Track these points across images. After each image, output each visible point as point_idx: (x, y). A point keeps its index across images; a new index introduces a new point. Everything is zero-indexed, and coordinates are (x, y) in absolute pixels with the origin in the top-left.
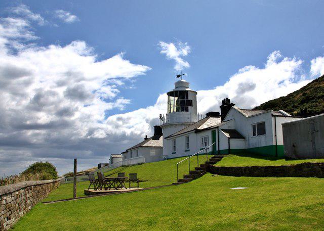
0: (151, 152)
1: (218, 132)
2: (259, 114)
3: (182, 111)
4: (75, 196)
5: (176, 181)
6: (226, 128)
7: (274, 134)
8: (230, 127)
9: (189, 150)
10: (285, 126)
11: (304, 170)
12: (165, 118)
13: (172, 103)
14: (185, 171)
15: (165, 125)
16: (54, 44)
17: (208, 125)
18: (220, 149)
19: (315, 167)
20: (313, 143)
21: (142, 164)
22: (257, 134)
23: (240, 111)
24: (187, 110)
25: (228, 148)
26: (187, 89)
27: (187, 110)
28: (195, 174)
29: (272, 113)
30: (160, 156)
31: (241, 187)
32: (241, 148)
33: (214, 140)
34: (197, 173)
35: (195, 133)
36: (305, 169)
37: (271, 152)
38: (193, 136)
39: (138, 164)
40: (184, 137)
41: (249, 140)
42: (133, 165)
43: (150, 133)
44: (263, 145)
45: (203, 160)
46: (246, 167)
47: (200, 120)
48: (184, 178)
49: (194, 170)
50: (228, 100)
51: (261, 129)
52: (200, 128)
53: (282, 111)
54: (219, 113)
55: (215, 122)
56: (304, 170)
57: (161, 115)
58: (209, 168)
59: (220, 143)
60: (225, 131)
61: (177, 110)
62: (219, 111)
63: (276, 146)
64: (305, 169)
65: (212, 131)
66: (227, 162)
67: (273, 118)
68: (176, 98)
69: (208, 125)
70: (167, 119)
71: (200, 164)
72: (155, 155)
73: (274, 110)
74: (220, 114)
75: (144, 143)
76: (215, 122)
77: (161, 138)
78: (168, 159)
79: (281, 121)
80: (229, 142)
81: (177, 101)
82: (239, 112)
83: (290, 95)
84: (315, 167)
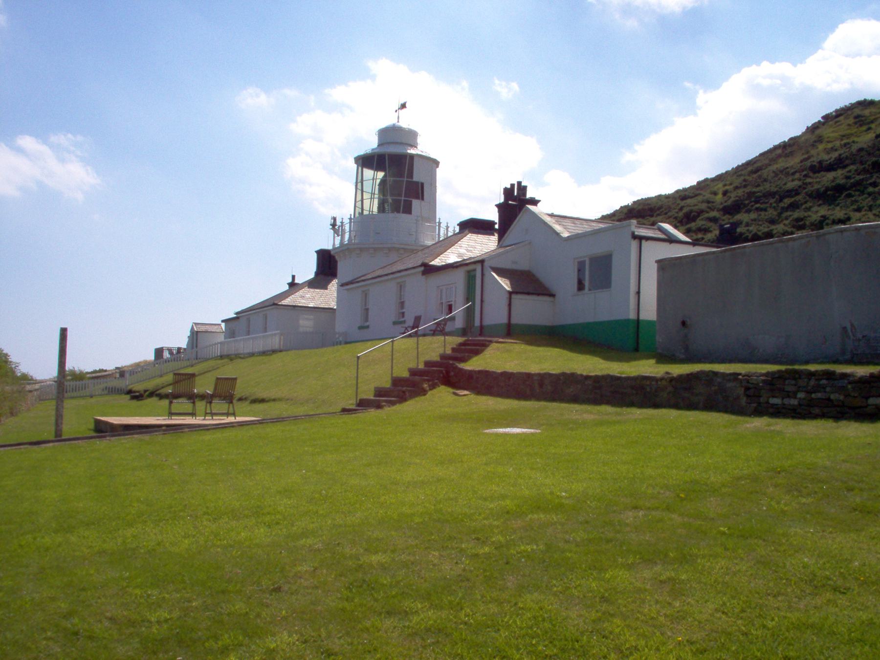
0: (301, 322)
1: (483, 275)
4: (58, 433)
5: (351, 404)
6: (508, 265)
7: (633, 288)
9: (368, 327)
10: (663, 265)
12: (347, 228)
13: (368, 187)
14: (379, 376)
15: (345, 249)
16: (768, 60)
17: (460, 255)
19: (730, 385)
21: (274, 351)
22: (587, 284)
23: (548, 220)
24: (408, 210)
26: (411, 151)
28: (404, 388)
29: (633, 228)
30: (324, 332)
31: (516, 426)
33: (469, 296)
34: (414, 384)
35: (424, 273)
37: (626, 339)
38: (417, 284)
39: (264, 353)
42: (252, 355)
43: (308, 270)
45: (435, 348)
46: (545, 374)
47: (450, 234)
48: (375, 396)
49: (406, 374)
50: (522, 189)
52: (437, 262)
53: (667, 226)
54: (493, 223)
55: (481, 246)
57: (335, 219)
58: (446, 374)
59: (485, 305)
60: (502, 272)
61: (382, 208)
62: (493, 215)
63: (638, 321)
65: (469, 272)
66: (502, 358)
67: (634, 244)
68: (381, 175)
69: (460, 255)
70: (350, 231)
71: (422, 359)
72: (311, 330)
73: (639, 223)
74: (497, 227)
75: (284, 295)
76: (481, 246)
77: (334, 285)
78: (346, 343)
79: (655, 253)
80: (510, 305)
81: (383, 182)
84: (730, 385)
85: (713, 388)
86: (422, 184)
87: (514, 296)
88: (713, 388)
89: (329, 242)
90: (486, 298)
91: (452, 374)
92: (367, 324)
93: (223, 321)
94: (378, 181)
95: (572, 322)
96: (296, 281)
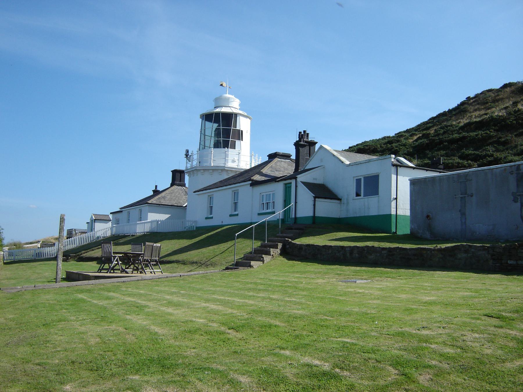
1: (296, 186)
2: (369, 161)
3: (224, 147)
8: (316, 179)
9: (237, 215)
11: (459, 256)
15: (193, 171)
18: (298, 215)
20: (463, 214)
23: (335, 153)
25: (311, 214)
27: (233, 147)
32: (176, 231)
35: (251, 185)
36: (461, 255)
40: (230, 190)
41: (348, 203)
43: (165, 181)
44: (373, 212)
51: (371, 185)
56: (459, 256)
64: (461, 255)
65: (286, 184)
80: (314, 205)
81: (217, 130)
82: (334, 155)
83: (399, 135)
85: (469, 255)
86: (242, 131)
87: (317, 199)
88: (469, 255)
89: (182, 166)
90: (298, 201)
91: (288, 246)
92: (236, 213)
93: (111, 213)
94: (214, 130)
95: (352, 216)
96: (158, 189)
